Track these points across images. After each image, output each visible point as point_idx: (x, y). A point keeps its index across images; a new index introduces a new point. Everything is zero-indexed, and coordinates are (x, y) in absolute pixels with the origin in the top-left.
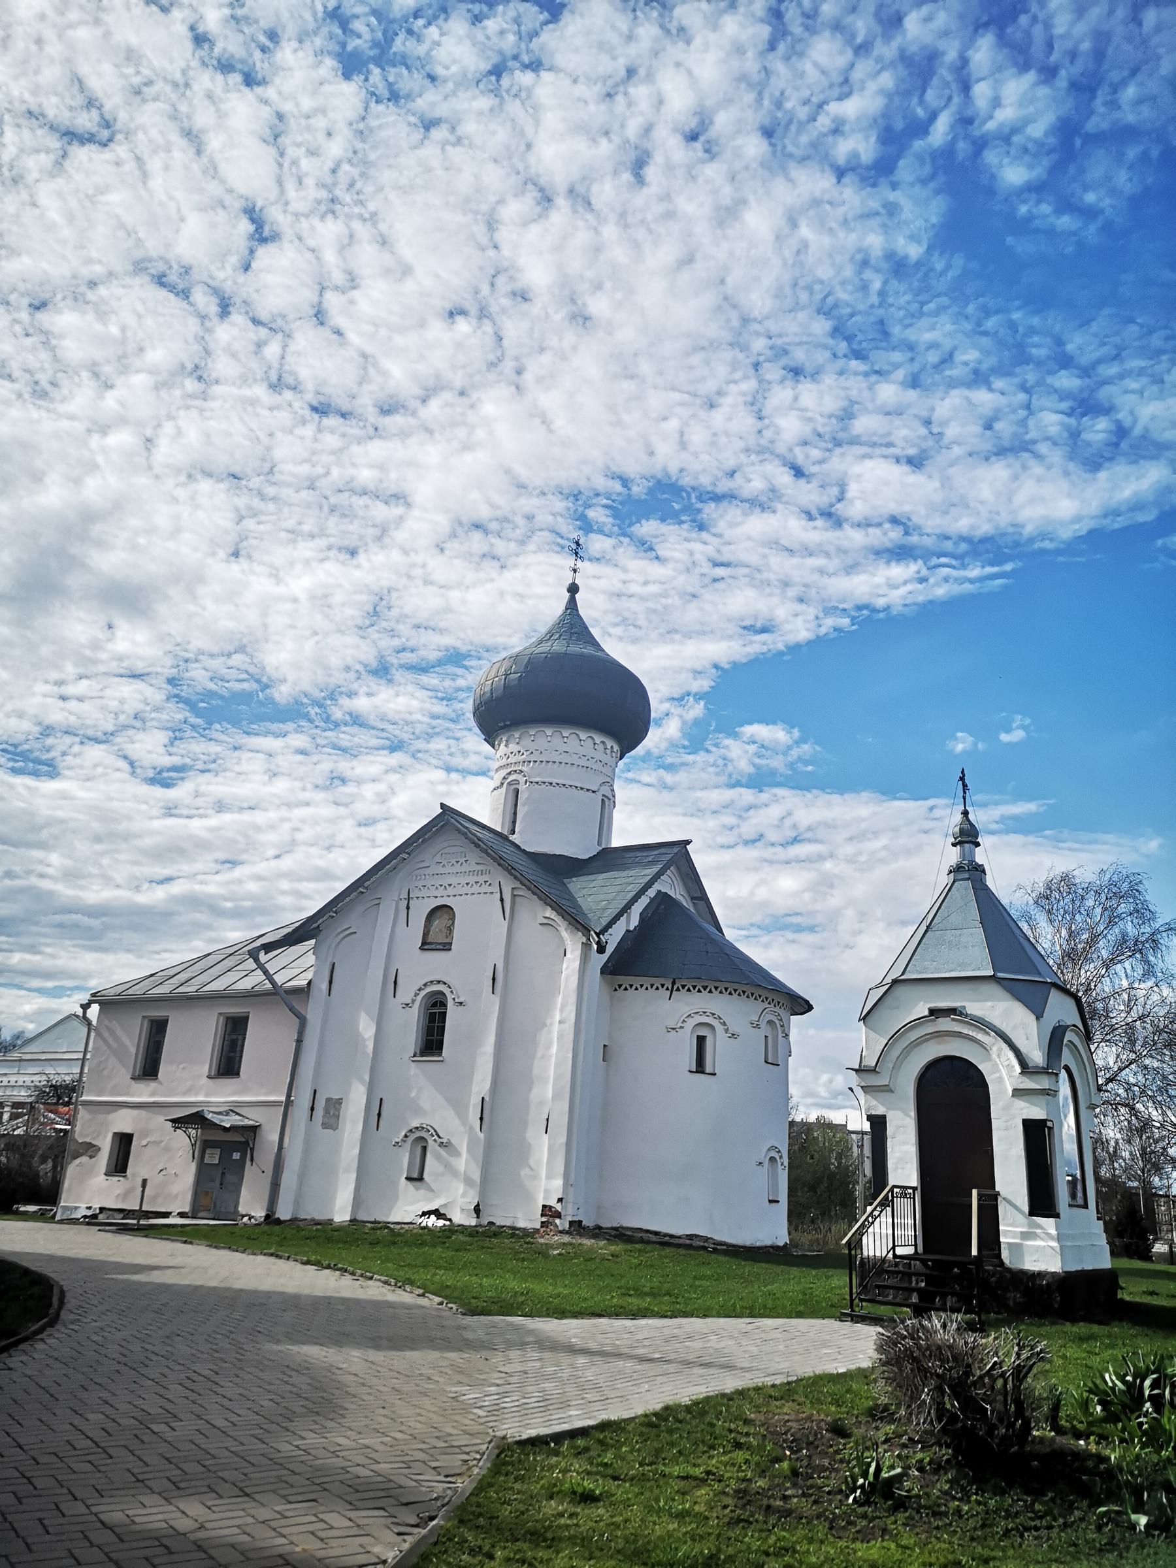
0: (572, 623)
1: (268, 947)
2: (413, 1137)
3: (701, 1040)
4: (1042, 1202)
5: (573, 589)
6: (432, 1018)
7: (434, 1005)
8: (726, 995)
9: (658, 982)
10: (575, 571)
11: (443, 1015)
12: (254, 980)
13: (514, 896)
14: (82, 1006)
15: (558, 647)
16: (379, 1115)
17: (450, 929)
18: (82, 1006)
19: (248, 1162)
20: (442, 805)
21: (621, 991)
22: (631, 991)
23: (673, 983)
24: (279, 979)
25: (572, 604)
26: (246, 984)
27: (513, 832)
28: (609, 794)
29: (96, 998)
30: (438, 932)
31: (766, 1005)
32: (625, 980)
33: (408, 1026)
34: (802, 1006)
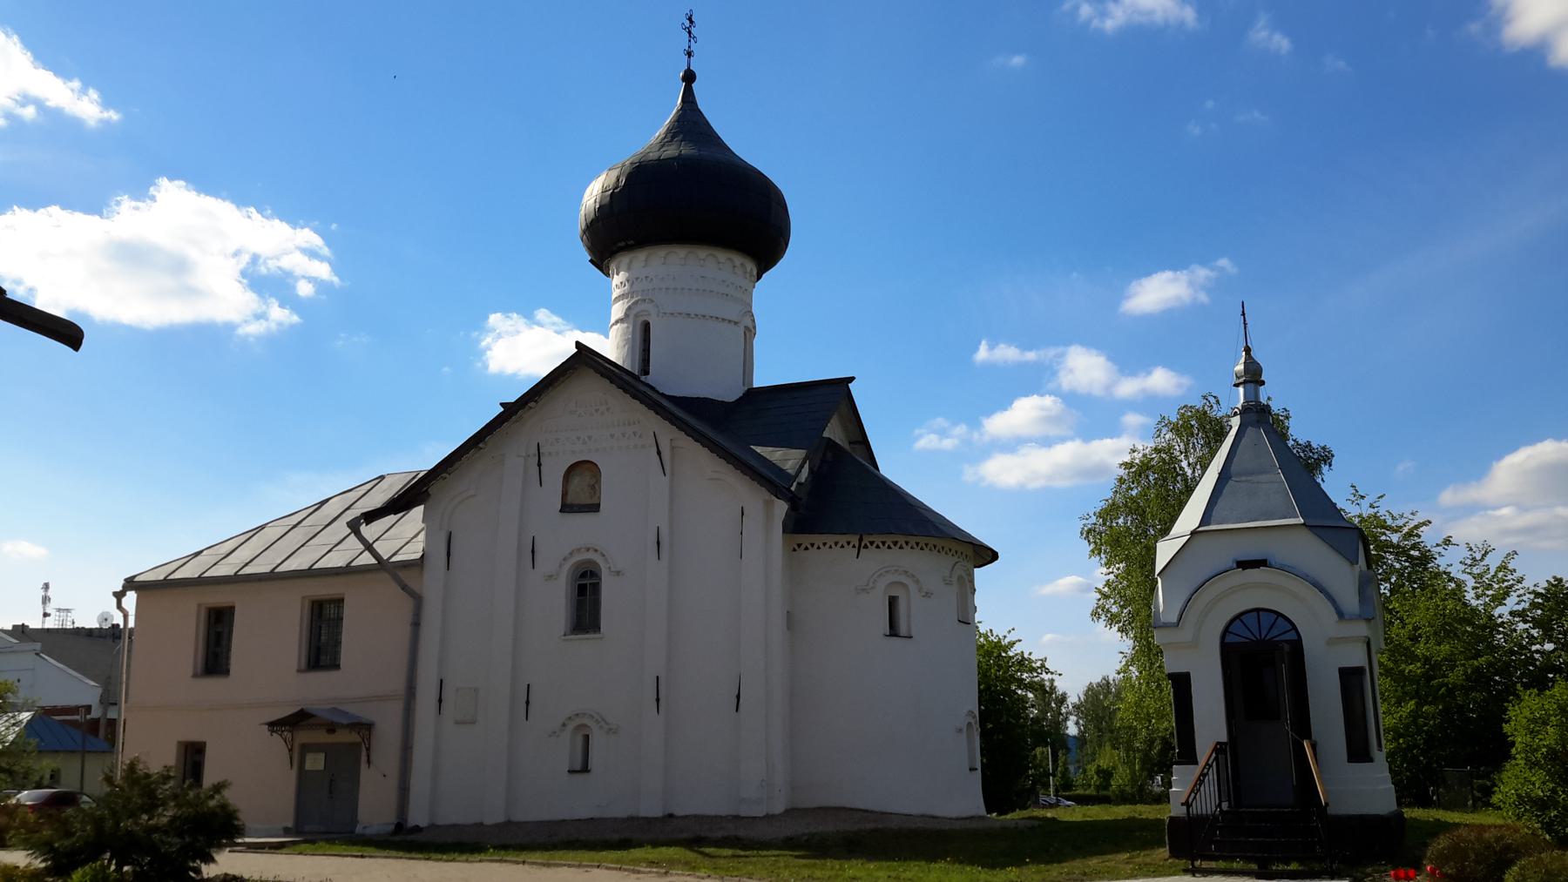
0: (690, 122)
1: (371, 517)
2: (571, 726)
3: (893, 602)
4: (1358, 752)
5: (689, 77)
6: (582, 590)
7: (584, 575)
8: (917, 550)
9: (843, 539)
10: (689, 54)
11: (596, 588)
12: (348, 553)
13: (673, 448)
14: (116, 594)
15: (671, 151)
16: (528, 703)
17: (595, 487)
18: (116, 594)
19: (364, 765)
20: (578, 344)
21: (801, 551)
22: (813, 551)
23: (861, 540)
24: (384, 549)
25: (689, 97)
26: (336, 560)
27: (647, 373)
28: (750, 325)
29: (130, 584)
30: (581, 492)
31: (956, 559)
32: (806, 539)
33: (557, 601)
34: (987, 555)
